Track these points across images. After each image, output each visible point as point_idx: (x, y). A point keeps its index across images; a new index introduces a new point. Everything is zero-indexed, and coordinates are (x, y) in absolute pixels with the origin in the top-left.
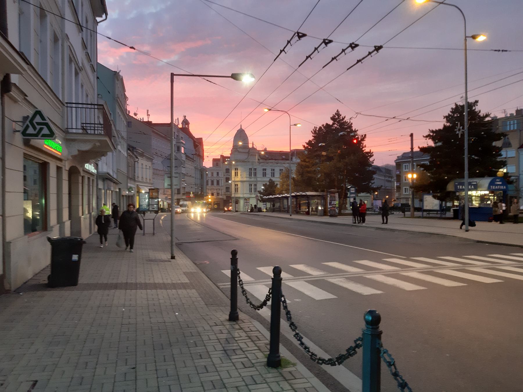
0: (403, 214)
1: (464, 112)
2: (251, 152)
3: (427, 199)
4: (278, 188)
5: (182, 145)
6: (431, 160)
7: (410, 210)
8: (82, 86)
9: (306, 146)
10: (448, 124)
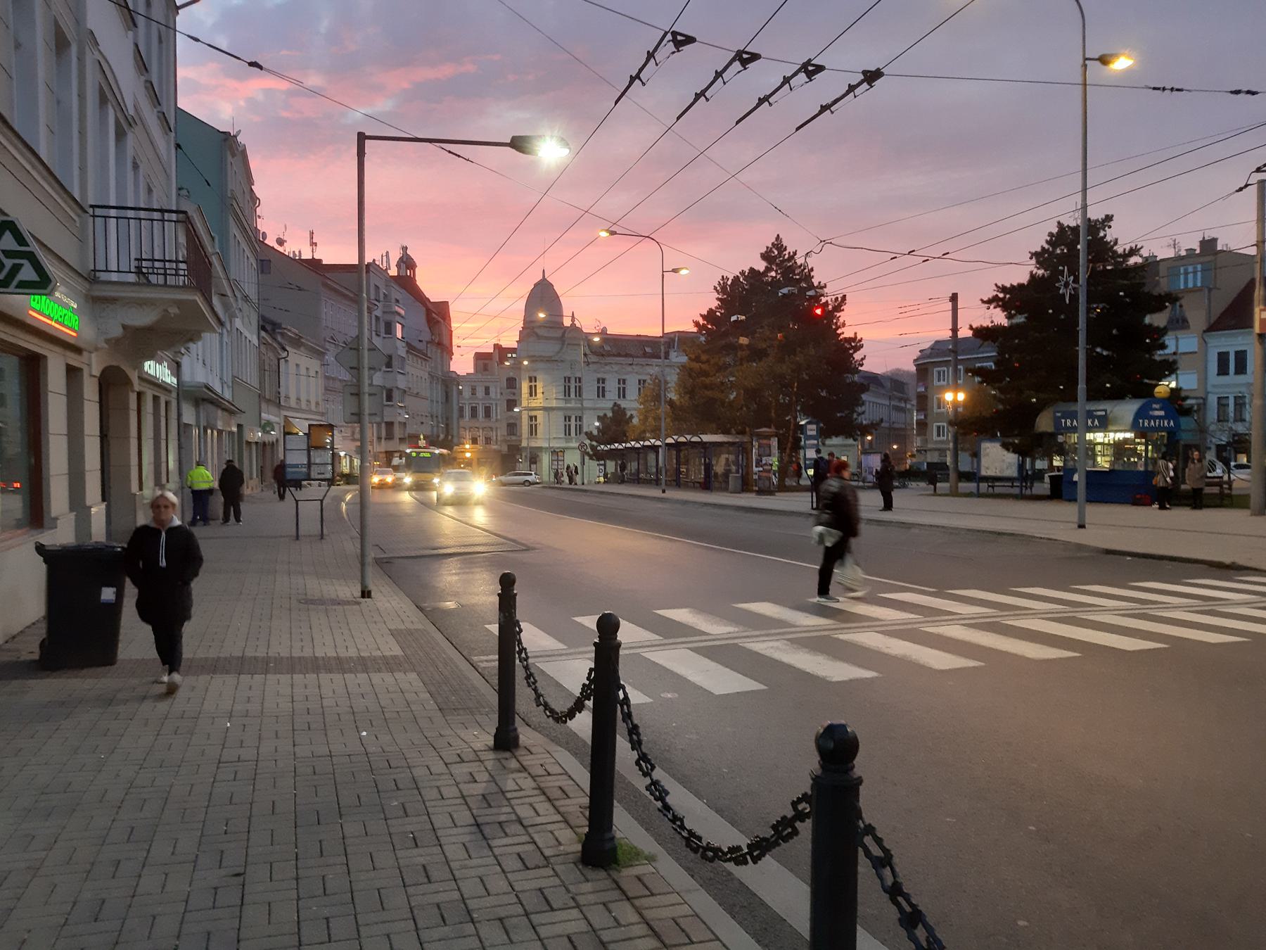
0: (932, 487)
1: (1078, 243)
2: (568, 336)
3: (988, 450)
4: (634, 426)
5: (398, 318)
6: (999, 358)
7: (948, 478)
8: (136, 166)
9: (701, 322)
10: (1041, 272)
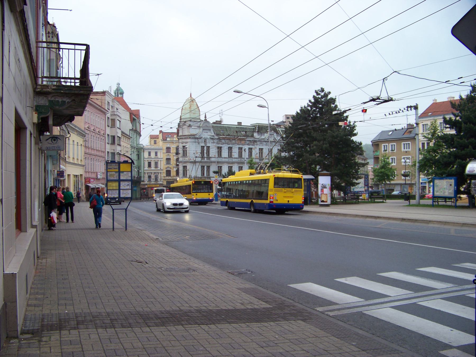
3: (438, 184)
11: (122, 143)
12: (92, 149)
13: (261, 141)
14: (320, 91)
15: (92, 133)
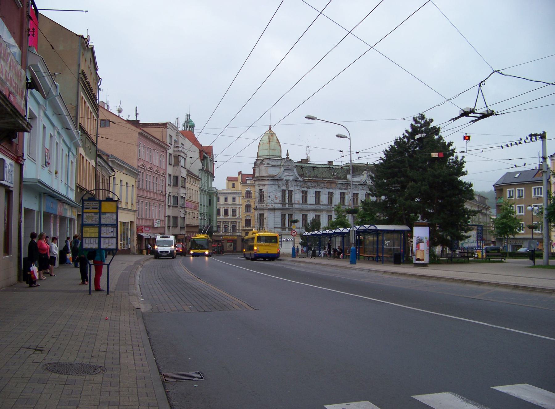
11: (187, 185)
12: (147, 191)
13: (356, 185)
14: (420, 119)
15: (148, 172)
